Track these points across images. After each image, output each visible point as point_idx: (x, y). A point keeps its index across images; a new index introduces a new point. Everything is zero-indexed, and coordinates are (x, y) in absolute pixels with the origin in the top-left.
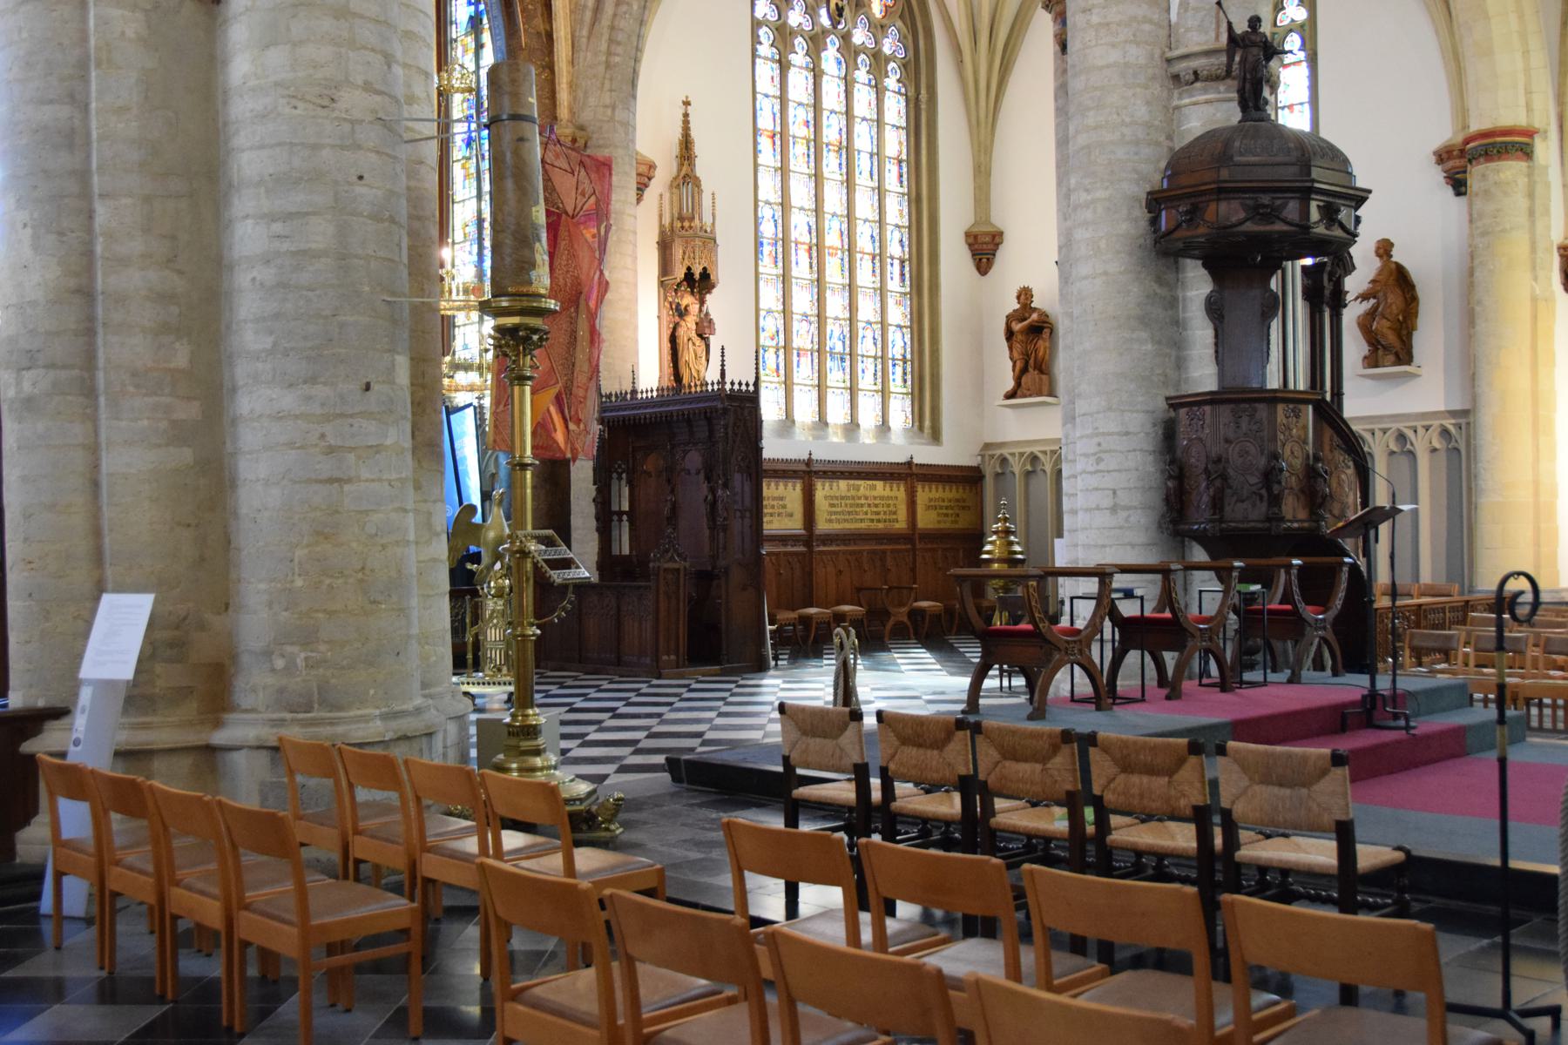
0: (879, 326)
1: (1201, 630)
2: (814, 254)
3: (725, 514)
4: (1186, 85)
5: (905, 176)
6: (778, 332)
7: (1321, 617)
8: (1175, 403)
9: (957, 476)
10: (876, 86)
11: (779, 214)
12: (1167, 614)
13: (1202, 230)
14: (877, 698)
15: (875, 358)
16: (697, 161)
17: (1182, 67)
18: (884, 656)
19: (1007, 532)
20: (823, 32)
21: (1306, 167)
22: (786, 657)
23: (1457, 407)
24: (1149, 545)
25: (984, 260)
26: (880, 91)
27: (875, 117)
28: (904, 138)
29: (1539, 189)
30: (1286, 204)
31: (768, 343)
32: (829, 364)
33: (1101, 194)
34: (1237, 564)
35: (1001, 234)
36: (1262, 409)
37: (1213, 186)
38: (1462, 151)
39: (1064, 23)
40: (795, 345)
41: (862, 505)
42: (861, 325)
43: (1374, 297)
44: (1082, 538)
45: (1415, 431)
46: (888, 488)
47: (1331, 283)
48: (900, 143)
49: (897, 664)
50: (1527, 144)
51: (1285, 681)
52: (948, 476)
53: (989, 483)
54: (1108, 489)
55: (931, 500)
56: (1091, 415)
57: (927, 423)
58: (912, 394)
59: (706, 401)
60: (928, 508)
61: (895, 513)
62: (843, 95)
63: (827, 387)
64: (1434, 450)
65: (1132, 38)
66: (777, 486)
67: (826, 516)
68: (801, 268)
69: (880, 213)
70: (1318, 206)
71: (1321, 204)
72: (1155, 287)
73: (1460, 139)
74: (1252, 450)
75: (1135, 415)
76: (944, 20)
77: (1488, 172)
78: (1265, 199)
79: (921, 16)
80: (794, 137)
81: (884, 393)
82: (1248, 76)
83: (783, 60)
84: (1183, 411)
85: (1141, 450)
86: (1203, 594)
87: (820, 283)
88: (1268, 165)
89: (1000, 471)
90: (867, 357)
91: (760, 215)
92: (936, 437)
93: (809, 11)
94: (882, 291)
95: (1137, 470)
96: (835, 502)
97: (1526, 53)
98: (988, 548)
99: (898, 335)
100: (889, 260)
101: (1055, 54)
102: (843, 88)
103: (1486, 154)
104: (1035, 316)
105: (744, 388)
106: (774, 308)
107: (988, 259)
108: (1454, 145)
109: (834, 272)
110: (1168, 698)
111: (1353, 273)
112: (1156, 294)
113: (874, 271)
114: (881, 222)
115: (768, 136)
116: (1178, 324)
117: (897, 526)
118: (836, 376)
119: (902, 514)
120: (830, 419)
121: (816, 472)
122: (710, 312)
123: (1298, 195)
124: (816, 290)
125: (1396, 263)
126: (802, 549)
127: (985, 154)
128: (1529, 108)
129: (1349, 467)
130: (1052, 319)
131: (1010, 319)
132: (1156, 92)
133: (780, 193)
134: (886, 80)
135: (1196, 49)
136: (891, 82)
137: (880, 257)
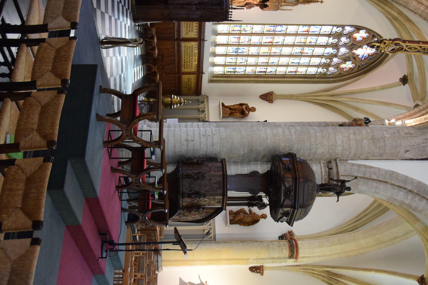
0: (246, 64)
1: (140, 179)
2: (269, 44)
3: (187, 8)
4: (328, 165)
5: (291, 73)
6: (246, 31)
7: (147, 218)
8: (223, 162)
9: (198, 87)
10: (320, 65)
11: (283, 32)
12: (146, 166)
13: (282, 172)
14: (122, 57)
15: (236, 63)
16: (303, 5)
17: (333, 164)
18: (140, 62)
19: (180, 103)
20: (338, 48)
21: (302, 207)
22: (140, 30)
23: (217, 237)
24: (175, 152)
25: (264, 97)
26: (318, 66)
27: (310, 65)
28: (303, 73)
29: (280, 260)
30: (290, 201)
31: (242, 28)
32: (235, 48)
33: (294, 137)
34: (165, 192)
35: (272, 102)
36: (220, 191)
37: (298, 176)
38: (292, 239)
39: (349, 126)
40: (241, 37)
41: (190, 57)
42: (246, 58)
43: (250, 213)
44: (177, 129)
45: (210, 225)
46: (195, 66)
47: (256, 203)
48: (302, 72)
49: (137, 67)
50: (293, 257)
51: (122, 207)
52: (198, 85)
53: (196, 98)
54: (194, 138)
55: (191, 79)
56: (220, 133)
57: (215, 79)
58: (224, 74)
59: (226, 3)
60: (189, 79)
61: (187, 68)
62: (318, 54)
63: (227, 47)
64: (204, 231)
65: (344, 148)
66: (196, 29)
67: (186, 45)
68: (266, 39)
69: (281, 65)
70: (289, 210)
71: (289, 211)
72: (262, 155)
73: (296, 238)
74: (207, 188)
75: (219, 148)
76: (337, 86)
77: (286, 246)
78: (292, 194)
79: (339, 80)
80: (307, 38)
81: (225, 65)
82: (331, 187)
83: (331, 35)
84: (220, 164)
85: (207, 150)
86: (154, 178)
87: (260, 45)
88: (304, 195)
89: (200, 101)
90: (236, 60)
91: (283, 26)
92: (211, 81)
93: (345, 44)
94: (256, 65)
95: (200, 148)
96: (191, 49)
97: (319, 256)
98: (176, 97)
99: (243, 70)
100: (266, 68)
101: (338, 122)
102: (320, 54)
103: (291, 246)
104: (247, 112)
105: (230, 16)
106: (253, 30)
107: (264, 98)
108: (294, 236)
109: (264, 50)
110: (112, 168)
111: (258, 209)
112: (260, 155)
113: (263, 63)
114: (278, 66)
115: (308, 30)
116: (249, 162)
117: (183, 69)
118: (231, 50)
119: (186, 70)
120: (217, 47)
121: (200, 43)
122: (254, 8)
123: (293, 204)
124: (258, 44)
125: (259, 220)
126: (176, 37)
127: (296, 98)
128: (303, 257)
129: (200, 218)
130: (246, 118)
131: (246, 105)
132: (326, 156)
133: (290, 33)
134: (321, 68)
135: (339, 169)
136: (320, 70)
137: (267, 65)
